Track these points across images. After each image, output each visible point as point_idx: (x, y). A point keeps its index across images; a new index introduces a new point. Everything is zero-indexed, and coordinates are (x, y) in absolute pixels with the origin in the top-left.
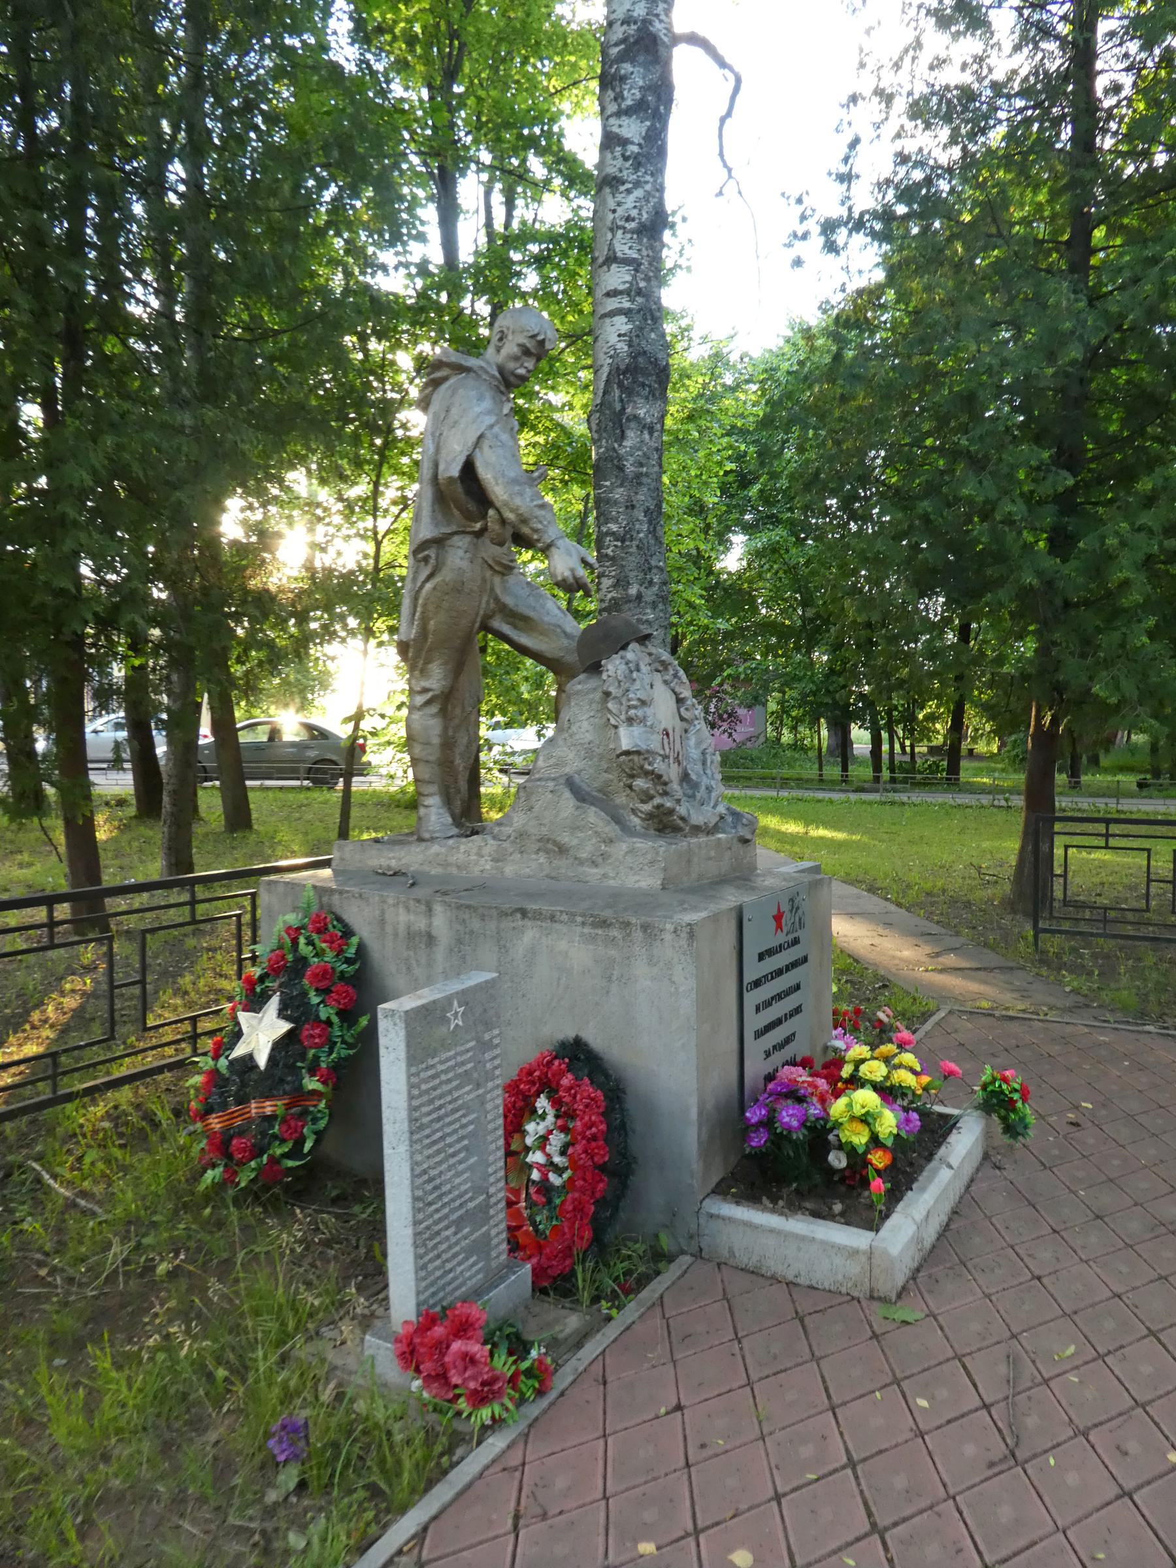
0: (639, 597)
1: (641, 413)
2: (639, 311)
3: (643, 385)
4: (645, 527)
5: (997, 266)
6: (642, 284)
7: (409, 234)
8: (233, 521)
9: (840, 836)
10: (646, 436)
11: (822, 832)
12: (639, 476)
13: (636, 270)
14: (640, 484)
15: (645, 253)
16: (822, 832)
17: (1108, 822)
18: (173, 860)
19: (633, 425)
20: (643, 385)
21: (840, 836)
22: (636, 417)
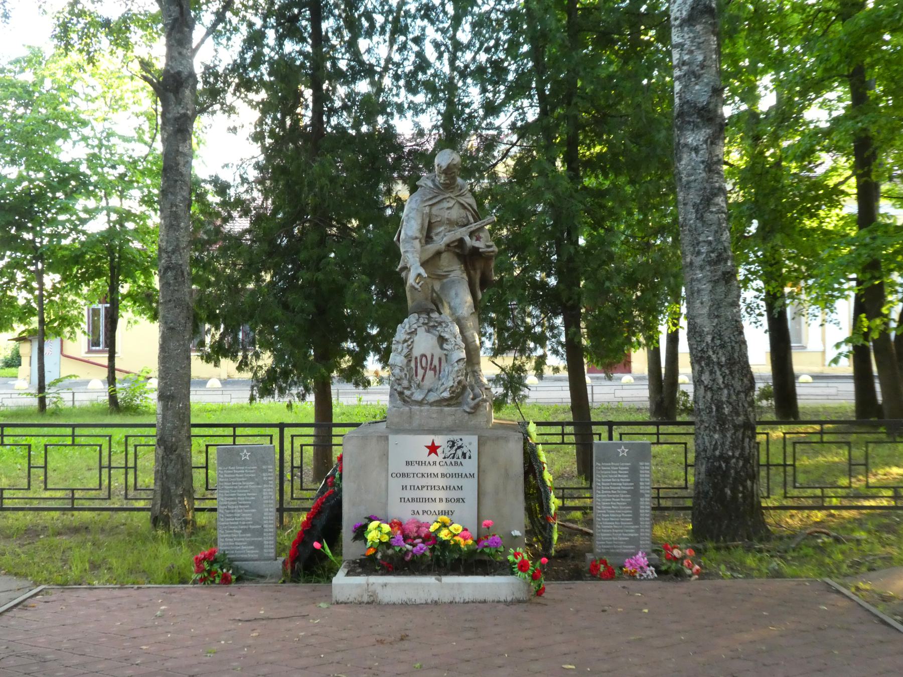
0: (691, 263)
1: (690, 140)
2: (685, 75)
3: (689, 122)
4: (694, 216)
5: (641, 210)
6: (686, 57)
7: (522, 120)
8: (263, 273)
9: (663, 371)
10: (693, 155)
11: (875, 368)
12: (688, 183)
13: (682, 50)
14: (689, 188)
15: (686, 36)
16: (875, 368)
17: (235, 426)
18: (476, 368)
19: (685, 149)
20: (689, 122)
21: (663, 371)
22: (686, 145)
